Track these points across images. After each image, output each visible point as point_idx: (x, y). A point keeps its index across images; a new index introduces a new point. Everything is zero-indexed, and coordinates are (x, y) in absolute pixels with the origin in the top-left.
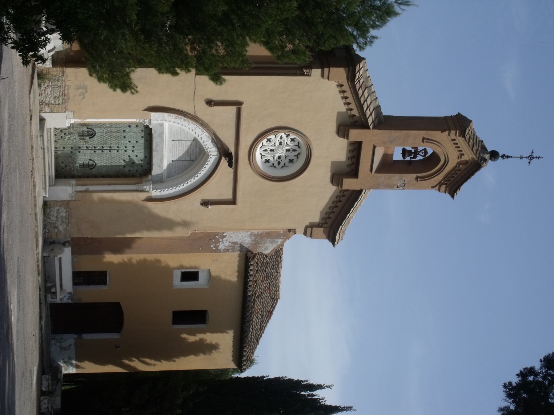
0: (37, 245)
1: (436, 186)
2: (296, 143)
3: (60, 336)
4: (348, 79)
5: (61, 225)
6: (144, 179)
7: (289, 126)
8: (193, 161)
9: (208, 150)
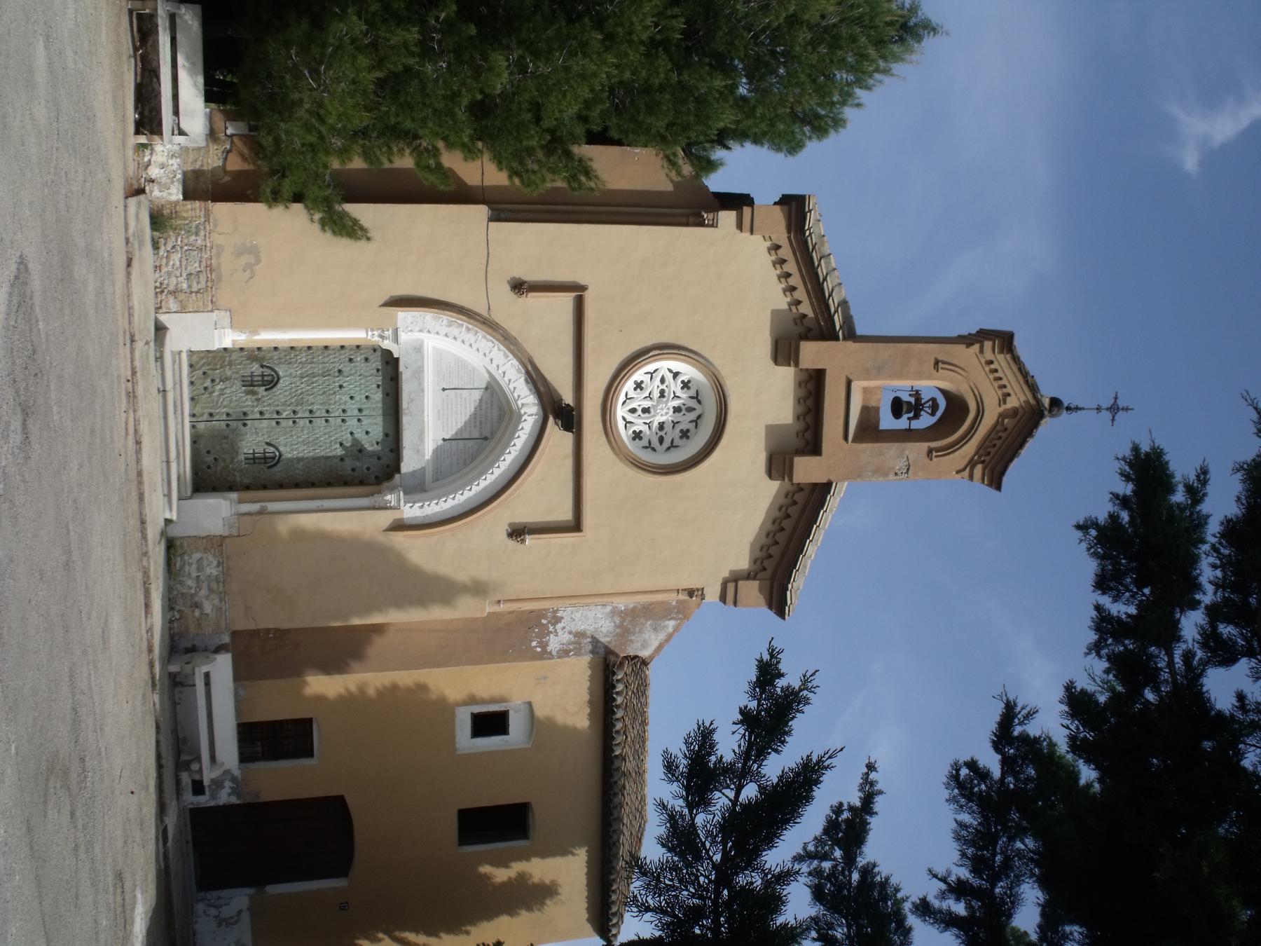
0: (147, 606)
1: (964, 469)
2: (692, 392)
3: (216, 893)
4: (789, 232)
5: (207, 597)
6: (386, 484)
7: (680, 343)
8: (486, 439)
9: (519, 403)
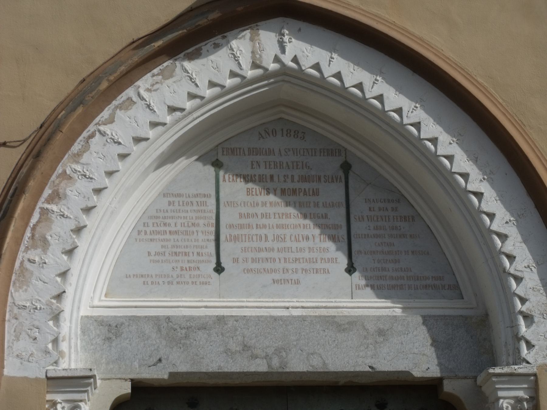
8: (346, 167)
9: (250, 74)
